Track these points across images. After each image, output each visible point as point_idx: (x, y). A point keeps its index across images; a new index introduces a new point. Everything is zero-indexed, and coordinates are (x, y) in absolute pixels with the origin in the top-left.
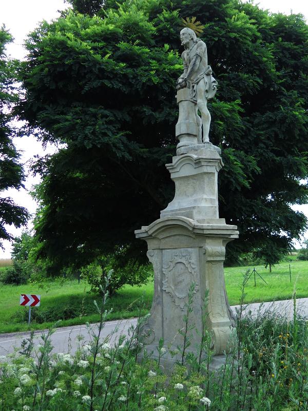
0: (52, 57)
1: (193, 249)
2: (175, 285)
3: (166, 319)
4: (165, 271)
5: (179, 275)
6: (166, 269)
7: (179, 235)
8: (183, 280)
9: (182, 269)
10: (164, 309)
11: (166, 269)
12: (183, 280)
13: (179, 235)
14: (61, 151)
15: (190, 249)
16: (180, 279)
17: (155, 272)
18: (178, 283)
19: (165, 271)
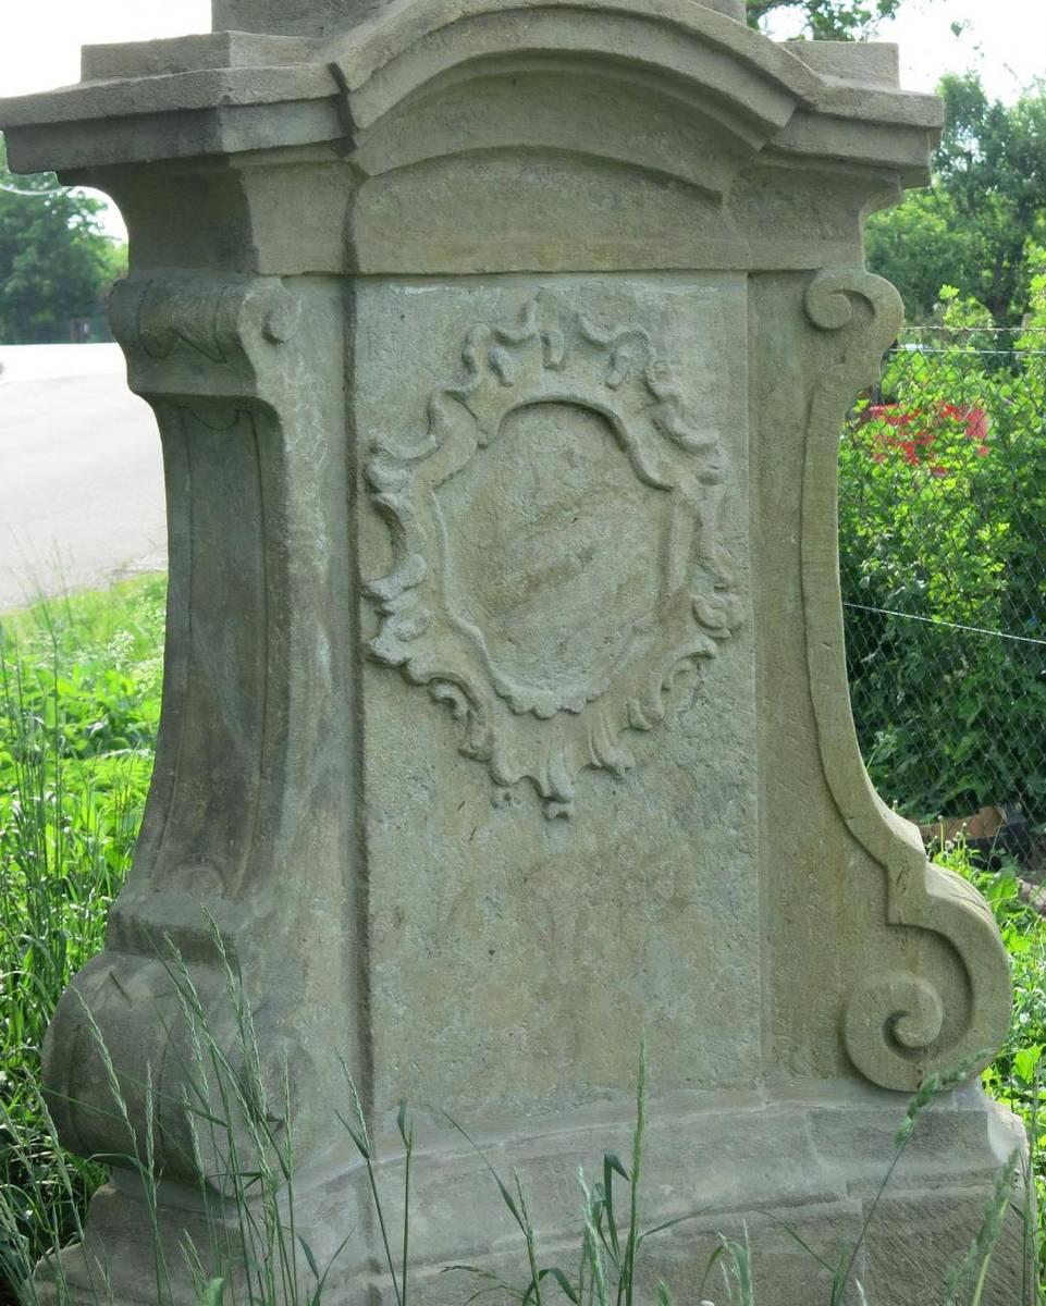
0: (966, 425)
1: (682, 290)
2: (500, 609)
3: (399, 918)
4: (401, 487)
5: (548, 516)
6: (410, 463)
7: (527, 153)
8: (587, 556)
9: (568, 456)
10: (381, 838)
11: (410, 463)
12: (587, 556)
13: (527, 153)
14: (791, 1215)
15: (645, 290)
16: (561, 545)
17: (408, 655)
18: (534, 584)
19: (401, 487)
